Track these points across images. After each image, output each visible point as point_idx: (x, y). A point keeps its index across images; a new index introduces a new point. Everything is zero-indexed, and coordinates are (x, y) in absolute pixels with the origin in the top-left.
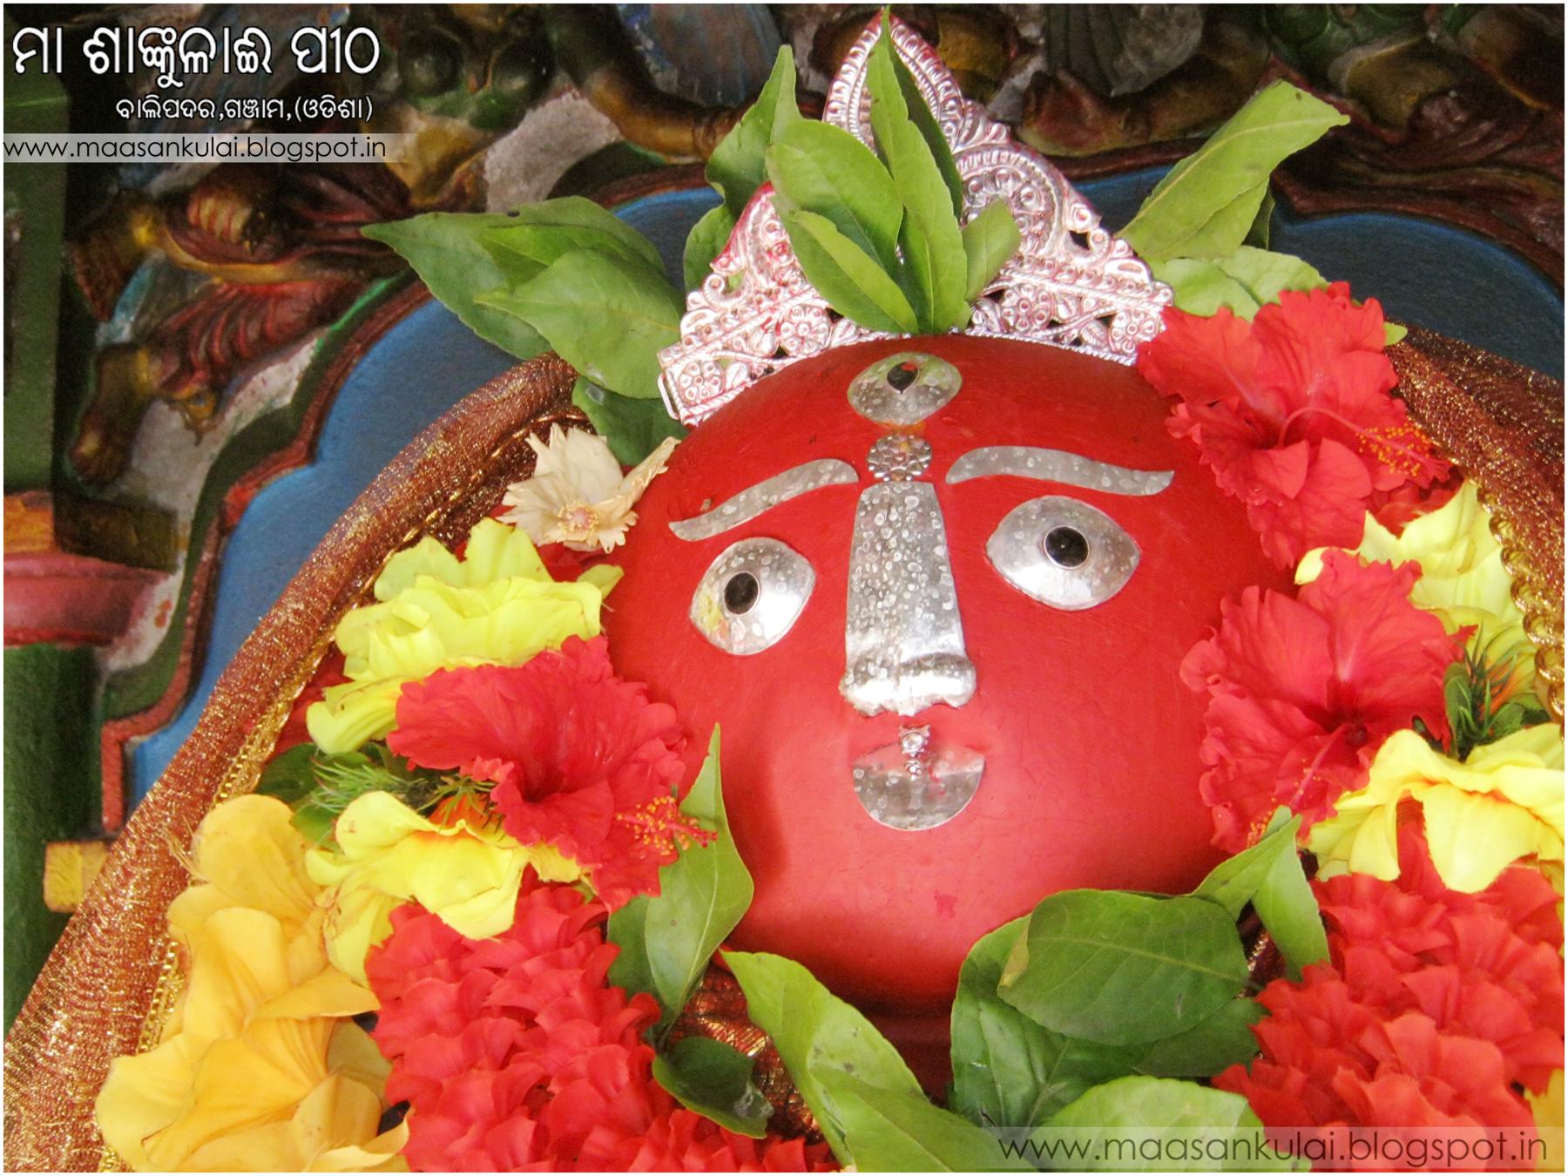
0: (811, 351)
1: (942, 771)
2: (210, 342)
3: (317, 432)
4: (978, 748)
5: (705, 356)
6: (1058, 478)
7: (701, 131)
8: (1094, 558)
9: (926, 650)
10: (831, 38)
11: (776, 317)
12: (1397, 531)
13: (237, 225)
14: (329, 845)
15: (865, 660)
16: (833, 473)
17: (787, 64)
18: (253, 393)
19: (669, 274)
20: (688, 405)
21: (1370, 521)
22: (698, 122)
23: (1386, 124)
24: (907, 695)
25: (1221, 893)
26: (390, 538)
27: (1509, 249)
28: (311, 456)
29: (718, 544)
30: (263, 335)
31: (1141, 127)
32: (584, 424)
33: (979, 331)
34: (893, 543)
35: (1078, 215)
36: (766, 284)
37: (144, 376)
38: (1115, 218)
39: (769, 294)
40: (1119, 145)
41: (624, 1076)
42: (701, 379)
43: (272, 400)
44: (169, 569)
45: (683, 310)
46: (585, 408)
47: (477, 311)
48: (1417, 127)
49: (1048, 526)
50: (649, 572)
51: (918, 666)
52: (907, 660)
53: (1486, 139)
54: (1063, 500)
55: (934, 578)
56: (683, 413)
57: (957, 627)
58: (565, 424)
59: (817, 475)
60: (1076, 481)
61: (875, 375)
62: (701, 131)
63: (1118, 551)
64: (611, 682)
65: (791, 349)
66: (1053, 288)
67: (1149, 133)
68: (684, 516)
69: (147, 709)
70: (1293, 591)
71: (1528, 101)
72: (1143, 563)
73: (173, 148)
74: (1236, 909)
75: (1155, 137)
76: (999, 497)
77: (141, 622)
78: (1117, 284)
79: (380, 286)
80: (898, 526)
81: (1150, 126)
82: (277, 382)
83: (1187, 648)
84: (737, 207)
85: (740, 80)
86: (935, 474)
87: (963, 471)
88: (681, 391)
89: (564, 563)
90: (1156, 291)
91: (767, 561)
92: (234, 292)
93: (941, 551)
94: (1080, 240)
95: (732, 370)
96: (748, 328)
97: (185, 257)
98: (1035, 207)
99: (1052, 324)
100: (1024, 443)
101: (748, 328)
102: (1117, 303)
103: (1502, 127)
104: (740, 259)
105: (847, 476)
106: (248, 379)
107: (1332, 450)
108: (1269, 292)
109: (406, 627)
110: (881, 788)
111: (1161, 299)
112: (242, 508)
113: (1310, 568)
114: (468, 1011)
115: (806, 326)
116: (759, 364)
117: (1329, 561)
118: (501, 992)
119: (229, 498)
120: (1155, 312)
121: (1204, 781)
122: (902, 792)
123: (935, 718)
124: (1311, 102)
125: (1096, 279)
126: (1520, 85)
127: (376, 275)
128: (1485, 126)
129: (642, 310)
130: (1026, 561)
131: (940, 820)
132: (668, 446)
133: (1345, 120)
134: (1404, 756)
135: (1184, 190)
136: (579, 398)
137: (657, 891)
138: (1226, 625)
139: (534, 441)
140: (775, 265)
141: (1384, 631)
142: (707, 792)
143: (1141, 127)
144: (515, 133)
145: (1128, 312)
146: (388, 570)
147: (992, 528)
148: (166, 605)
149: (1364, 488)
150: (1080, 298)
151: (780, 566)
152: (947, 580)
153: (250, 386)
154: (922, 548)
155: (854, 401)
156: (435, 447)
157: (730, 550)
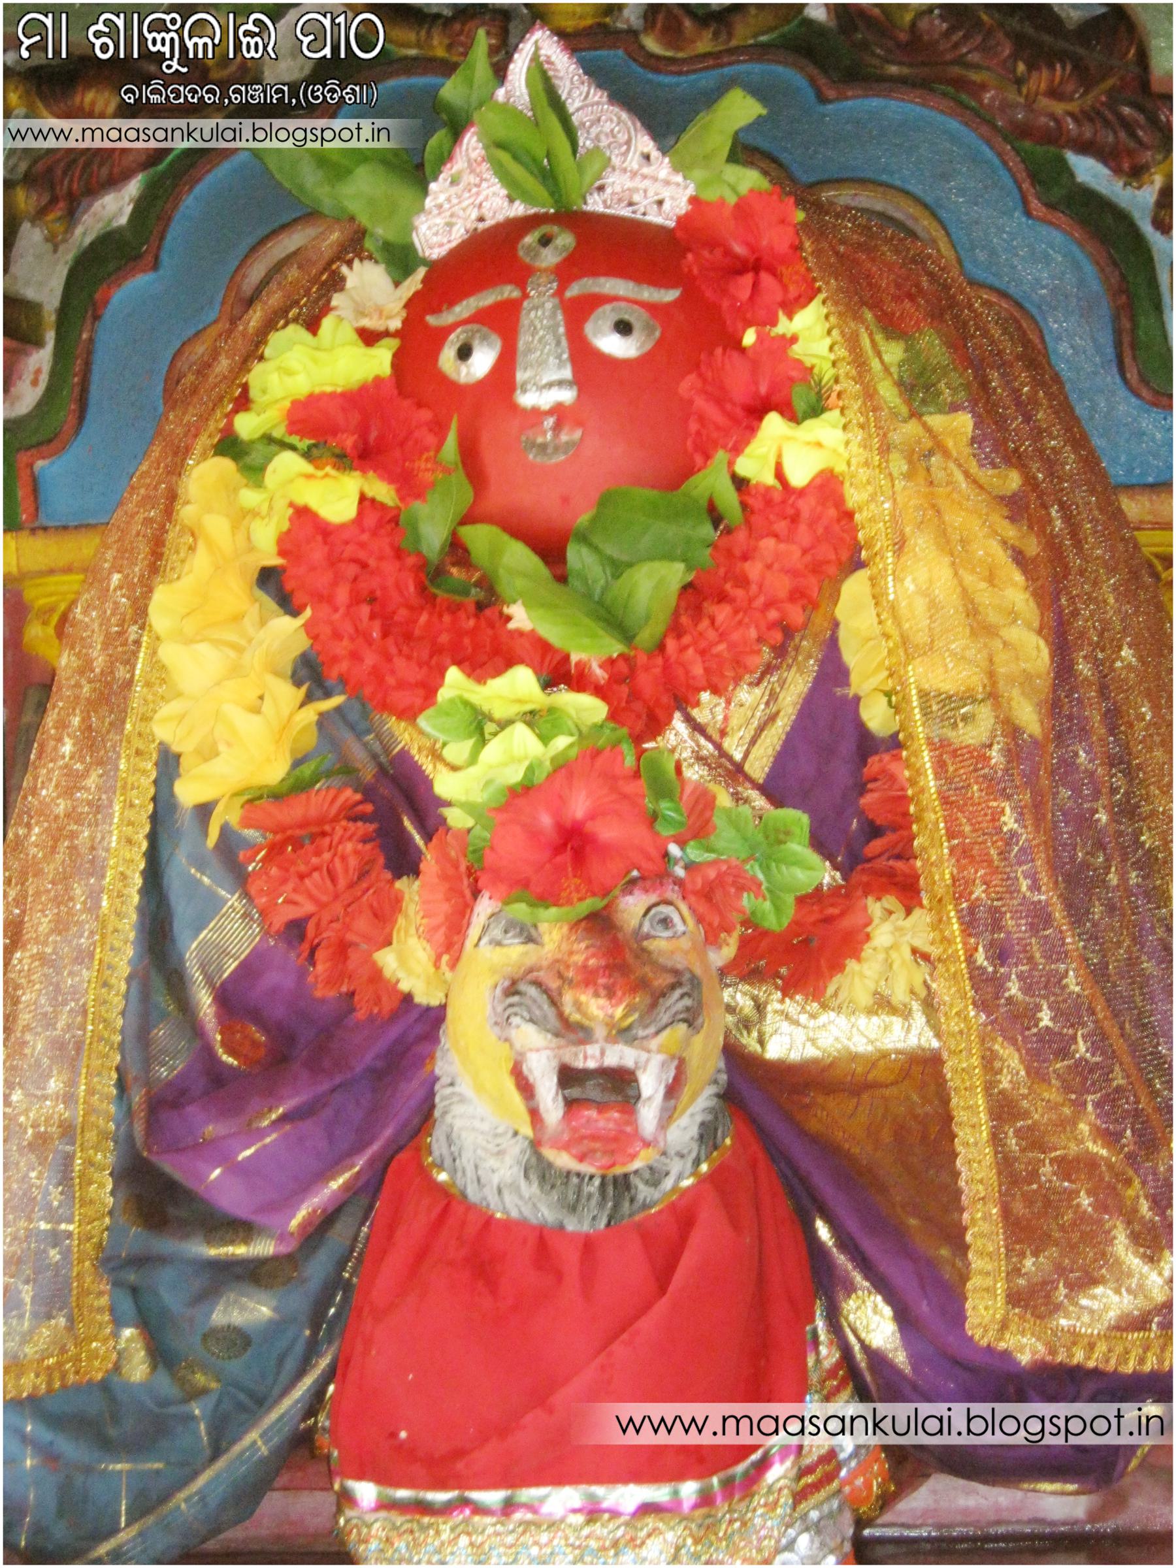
0: (500, 218)
1: (564, 438)
2: (71, 181)
3: (159, 248)
5: (439, 221)
6: (621, 293)
8: (636, 332)
10: (507, 27)
14: (259, 485)
16: (509, 292)
17: (482, 41)
19: (415, 170)
21: (781, 313)
22: (420, 25)
25: (695, 493)
26: (270, 325)
28: (155, 266)
31: (723, 37)
32: (370, 258)
33: (589, 208)
35: (645, 143)
37: (22, 206)
40: (708, 49)
41: (412, 589)
42: (436, 234)
43: (110, 221)
44: (39, 344)
45: (425, 192)
47: (301, 187)
49: (615, 317)
50: (416, 343)
51: (550, 385)
52: (545, 386)
54: (623, 304)
55: (558, 343)
61: (530, 239)
62: (423, 33)
63: (649, 330)
67: (729, 39)
69: (50, 441)
70: (743, 351)
72: (663, 333)
73: (178, 133)
74: (704, 503)
75: (734, 43)
76: (594, 302)
77: (19, 384)
78: (667, 183)
80: (541, 318)
81: (730, 35)
83: (683, 377)
84: (457, 132)
86: (560, 293)
87: (574, 291)
89: (369, 337)
90: (686, 187)
93: (562, 330)
94: (647, 157)
95: (455, 229)
98: (623, 137)
99: (631, 204)
102: (665, 193)
104: (459, 164)
105: (516, 294)
106: (90, 206)
107: (766, 278)
108: (744, 189)
109: (290, 373)
110: (533, 445)
112: (106, 302)
113: (749, 338)
114: (333, 561)
115: (495, 203)
116: (471, 225)
117: (759, 334)
118: (349, 551)
119: (97, 296)
120: (685, 199)
121: (689, 443)
122: (543, 447)
123: (558, 410)
129: (404, 194)
130: (604, 335)
131: (563, 457)
132: (421, 272)
133: (764, 112)
134: (773, 422)
136: (369, 244)
137: (425, 501)
138: (703, 368)
139: (344, 269)
142: (450, 449)
143: (723, 36)
148: (38, 372)
149: (779, 297)
150: (645, 191)
151: (484, 338)
152: (564, 343)
153: (93, 209)
154: (553, 329)
155: (521, 253)
157: (459, 330)
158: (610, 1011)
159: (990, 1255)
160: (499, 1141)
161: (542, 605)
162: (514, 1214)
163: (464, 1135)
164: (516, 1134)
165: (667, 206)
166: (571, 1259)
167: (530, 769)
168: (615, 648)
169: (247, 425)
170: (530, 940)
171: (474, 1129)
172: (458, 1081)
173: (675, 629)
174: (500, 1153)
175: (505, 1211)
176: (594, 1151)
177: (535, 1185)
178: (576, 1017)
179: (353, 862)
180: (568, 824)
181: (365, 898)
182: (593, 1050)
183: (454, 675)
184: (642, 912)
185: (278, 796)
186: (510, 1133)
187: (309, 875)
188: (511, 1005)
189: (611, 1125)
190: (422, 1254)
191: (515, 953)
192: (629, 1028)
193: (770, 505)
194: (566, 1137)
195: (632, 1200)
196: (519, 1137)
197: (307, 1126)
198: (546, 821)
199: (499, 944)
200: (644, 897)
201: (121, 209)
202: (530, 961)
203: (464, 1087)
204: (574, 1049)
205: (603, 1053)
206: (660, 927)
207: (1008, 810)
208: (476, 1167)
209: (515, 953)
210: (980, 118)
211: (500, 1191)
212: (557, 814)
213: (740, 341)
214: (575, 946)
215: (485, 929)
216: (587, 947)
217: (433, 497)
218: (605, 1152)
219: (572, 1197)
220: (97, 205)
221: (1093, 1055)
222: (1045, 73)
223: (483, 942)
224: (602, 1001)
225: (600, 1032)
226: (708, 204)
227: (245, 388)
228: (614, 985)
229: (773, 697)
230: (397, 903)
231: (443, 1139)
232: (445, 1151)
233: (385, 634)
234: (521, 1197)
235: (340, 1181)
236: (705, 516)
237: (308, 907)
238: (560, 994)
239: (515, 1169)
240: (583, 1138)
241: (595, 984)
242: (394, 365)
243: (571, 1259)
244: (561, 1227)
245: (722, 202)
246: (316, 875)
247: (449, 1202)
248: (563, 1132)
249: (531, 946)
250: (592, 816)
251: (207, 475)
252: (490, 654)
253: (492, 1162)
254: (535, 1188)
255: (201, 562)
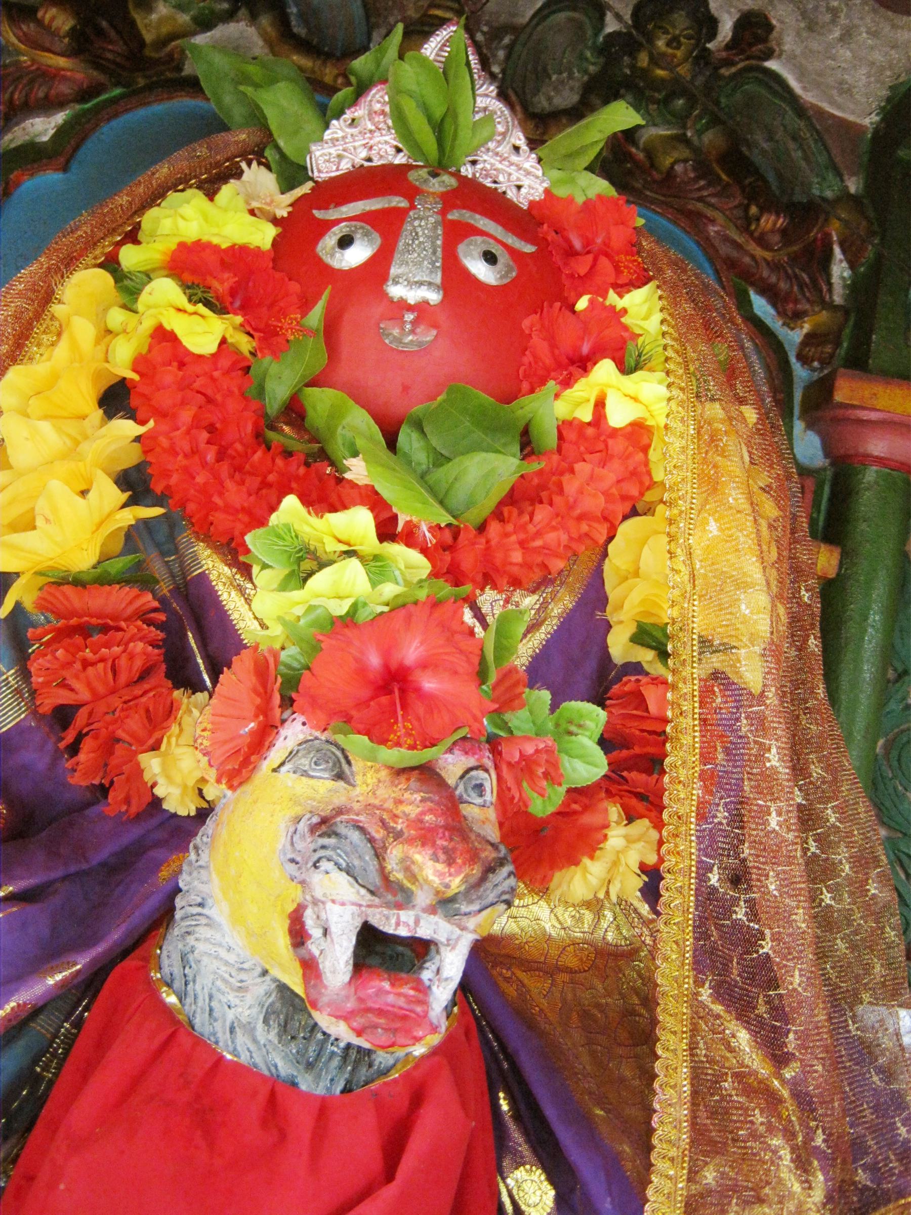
4: (435, 326)
5: (333, 151)
6: (492, 232)
7: (319, 62)
9: (425, 279)
11: (372, 142)
12: (621, 297)
13: (67, 27)
15: (398, 276)
18: (24, 129)
20: (319, 171)
23: (656, 169)
24: (413, 296)
26: (179, 184)
27: (698, 244)
28: (65, 169)
29: (337, 222)
30: (47, 97)
32: (268, 167)
34: (420, 233)
35: (519, 139)
36: (370, 126)
38: (533, 144)
39: (371, 131)
45: (327, 127)
46: (270, 159)
48: (670, 174)
49: (485, 248)
50: (299, 232)
51: (420, 284)
52: (414, 284)
53: (699, 189)
54: (492, 241)
55: (434, 253)
56: (316, 174)
57: (439, 274)
58: (260, 163)
59: (390, 202)
60: (499, 237)
64: (271, 271)
65: (375, 159)
66: (500, 166)
68: (319, 208)
71: (724, 177)
74: (521, 426)
76: (467, 231)
79: (117, 91)
82: (42, 127)
85: (340, 44)
86: (443, 213)
88: (317, 165)
90: (543, 181)
91: (360, 231)
92: (34, 68)
93: (439, 242)
94: (517, 149)
96: (357, 144)
97: (14, 40)
100: (481, 214)
101: (357, 144)
102: (526, 182)
103: (709, 184)
104: (359, 112)
105: (403, 204)
107: (604, 262)
108: (592, 194)
111: (545, 185)
112: (18, 184)
113: (582, 304)
114: (184, 386)
116: (358, 161)
117: (591, 302)
120: (541, 190)
123: (421, 308)
124: (631, 111)
125: (519, 168)
126: (723, 170)
127: (117, 84)
128: (702, 183)
129: (309, 118)
130: (473, 258)
132: (310, 184)
134: (605, 369)
135: (565, 139)
139: (244, 165)
140: (377, 119)
141: (607, 332)
142: (316, 316)
144: (209, 34)
145: (530, 187)
146: (168, 199)
147: (461, 241)
149: (612, 279)
150: (510, 174)
151: (366, 234)
153: (23, 125)
156: (201, 151)
157: (343, 224)
158: (447, 880)
159: (672, 1160)
160: (243, 976)
161: (382, 465)
162: (244, 1059)
163: (205, 960)
164: (265, 973)
165: (523, 191)
166: (302, 1123)
167: (355, 607)
168: (445, 519)
169: (129, 257)
170: (340, 776)
171: (217, 957)
172: (210, 902)
173: (498, 514)
174: (241, 989)
175: (235, 1052)
176: (376, 1027)
177: (274, 1032)
178: (398, 875)
179: (138, 663)
180: (394, 666)
181: (144, 699)
182: (407, 916)
183: (291, 502)
184: (460, 773)
185: (78, 582)
186: (259, 970)
187: (93, 664)
188: (323, 847)
189: (401, 1002)
190: (136, 1082)
191: (322, 790)
192: (452, 900)
193: (591, 436)
194: (350, 1005)
195: (370, 1065)
196: (267, 978)
197: (32, 909)
198: (374, 660)
199: (305, 774)
200: (463, 758)
201: (46, 130)
202: (339, 800)
203: (218, 911)
204: (386, 911)
205: (417, 922)
206: (473, 794)
207: (774, 750)
208: (211, 997)
209: (322, 790)
210: (707, 245)
211: (232, 1030)
212: (386, 654)
213: (574, 305)
214: (407, 795)
215: (292, 755)
216: (423, 800)
217: (288, 357)
218: (386, 1030)
219: (311, 1054)
220: (28, 122)
221: (805, 990)
222: (773, 218)
223: (283, 769)
224: (440, 867)
225: (423, 898)
226: (558, 199)
227: (137, 227)
228: (454, 850)
229: (544, 606)
230: (170, 711)
231: (176, 957)
232: (177, 971)
233: (219, 460)
234: (255, 1041)
235: (59, 977)
236: (518, 438)
237: (84, 695)
238: (385, 848)
239: (255, 1010)
240: (368, 1010)
241: (434, 844)
242: (275, 243)
243: (302, 1123)
244: (294, 1085)
245: (570, 200)
246: (100, 666)
247: (175, 1031)
248: (347, 997)
249: (341, 784)
250: (424, 665)
251: (86, 284)
252: (326, 495)
253: (232, 997)
254: (273, 1036)
255: (62, 351)
